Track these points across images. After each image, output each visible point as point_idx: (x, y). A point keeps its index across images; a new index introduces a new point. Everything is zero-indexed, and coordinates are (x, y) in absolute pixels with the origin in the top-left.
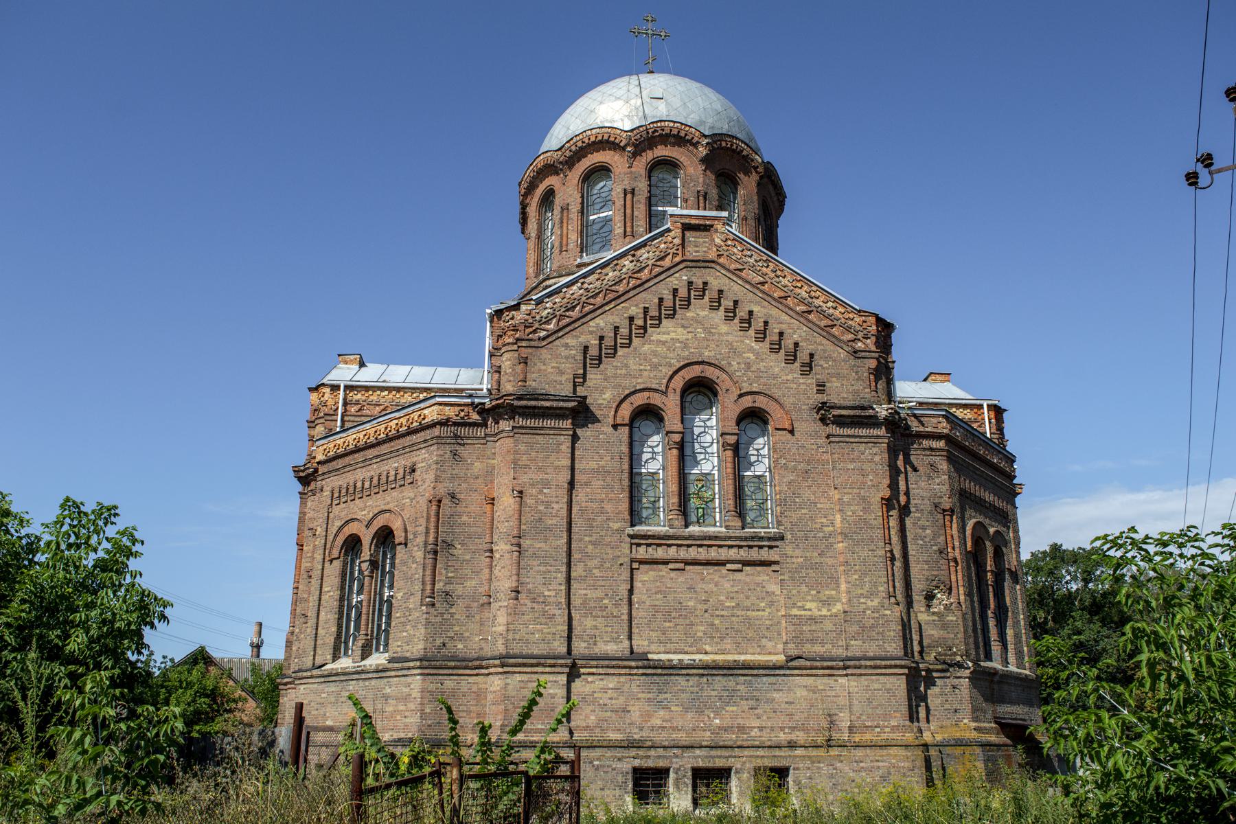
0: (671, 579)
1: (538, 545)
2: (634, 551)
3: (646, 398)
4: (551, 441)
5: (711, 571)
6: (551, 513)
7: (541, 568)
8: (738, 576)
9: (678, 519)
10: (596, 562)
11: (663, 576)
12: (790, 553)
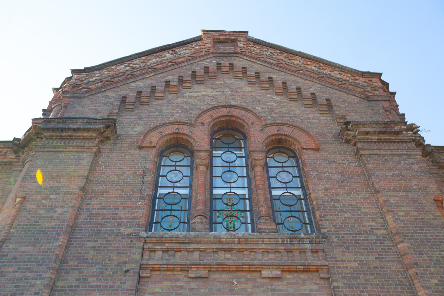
0: (191, 290)
1: (24, 249)
2: (146, 257)
3: (175, 128)
4: (72, 157)
5: (242, 280)
6: (52, 216)
7: (17, 274)
8: (277, 285)
9: (201, 223)
10: (95, 269)
11: (181, 286)
12: (340, 257)
